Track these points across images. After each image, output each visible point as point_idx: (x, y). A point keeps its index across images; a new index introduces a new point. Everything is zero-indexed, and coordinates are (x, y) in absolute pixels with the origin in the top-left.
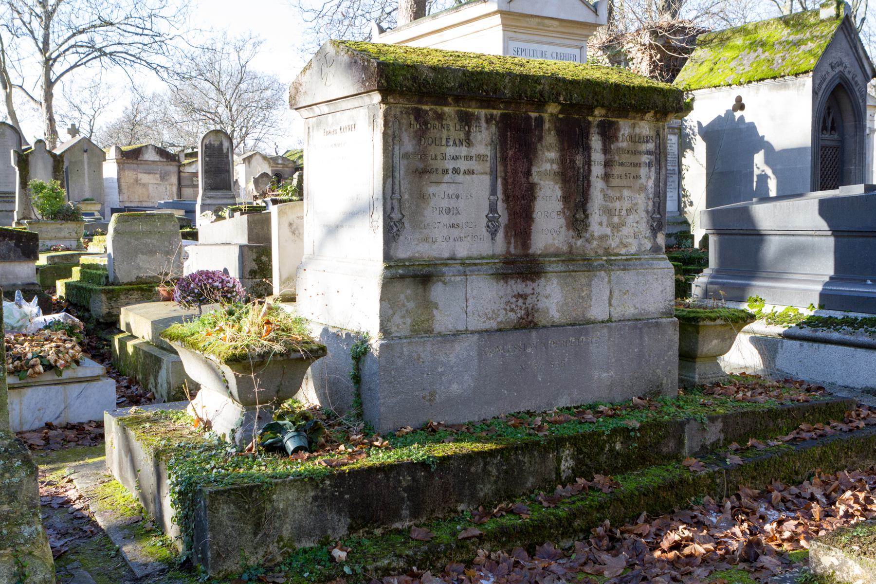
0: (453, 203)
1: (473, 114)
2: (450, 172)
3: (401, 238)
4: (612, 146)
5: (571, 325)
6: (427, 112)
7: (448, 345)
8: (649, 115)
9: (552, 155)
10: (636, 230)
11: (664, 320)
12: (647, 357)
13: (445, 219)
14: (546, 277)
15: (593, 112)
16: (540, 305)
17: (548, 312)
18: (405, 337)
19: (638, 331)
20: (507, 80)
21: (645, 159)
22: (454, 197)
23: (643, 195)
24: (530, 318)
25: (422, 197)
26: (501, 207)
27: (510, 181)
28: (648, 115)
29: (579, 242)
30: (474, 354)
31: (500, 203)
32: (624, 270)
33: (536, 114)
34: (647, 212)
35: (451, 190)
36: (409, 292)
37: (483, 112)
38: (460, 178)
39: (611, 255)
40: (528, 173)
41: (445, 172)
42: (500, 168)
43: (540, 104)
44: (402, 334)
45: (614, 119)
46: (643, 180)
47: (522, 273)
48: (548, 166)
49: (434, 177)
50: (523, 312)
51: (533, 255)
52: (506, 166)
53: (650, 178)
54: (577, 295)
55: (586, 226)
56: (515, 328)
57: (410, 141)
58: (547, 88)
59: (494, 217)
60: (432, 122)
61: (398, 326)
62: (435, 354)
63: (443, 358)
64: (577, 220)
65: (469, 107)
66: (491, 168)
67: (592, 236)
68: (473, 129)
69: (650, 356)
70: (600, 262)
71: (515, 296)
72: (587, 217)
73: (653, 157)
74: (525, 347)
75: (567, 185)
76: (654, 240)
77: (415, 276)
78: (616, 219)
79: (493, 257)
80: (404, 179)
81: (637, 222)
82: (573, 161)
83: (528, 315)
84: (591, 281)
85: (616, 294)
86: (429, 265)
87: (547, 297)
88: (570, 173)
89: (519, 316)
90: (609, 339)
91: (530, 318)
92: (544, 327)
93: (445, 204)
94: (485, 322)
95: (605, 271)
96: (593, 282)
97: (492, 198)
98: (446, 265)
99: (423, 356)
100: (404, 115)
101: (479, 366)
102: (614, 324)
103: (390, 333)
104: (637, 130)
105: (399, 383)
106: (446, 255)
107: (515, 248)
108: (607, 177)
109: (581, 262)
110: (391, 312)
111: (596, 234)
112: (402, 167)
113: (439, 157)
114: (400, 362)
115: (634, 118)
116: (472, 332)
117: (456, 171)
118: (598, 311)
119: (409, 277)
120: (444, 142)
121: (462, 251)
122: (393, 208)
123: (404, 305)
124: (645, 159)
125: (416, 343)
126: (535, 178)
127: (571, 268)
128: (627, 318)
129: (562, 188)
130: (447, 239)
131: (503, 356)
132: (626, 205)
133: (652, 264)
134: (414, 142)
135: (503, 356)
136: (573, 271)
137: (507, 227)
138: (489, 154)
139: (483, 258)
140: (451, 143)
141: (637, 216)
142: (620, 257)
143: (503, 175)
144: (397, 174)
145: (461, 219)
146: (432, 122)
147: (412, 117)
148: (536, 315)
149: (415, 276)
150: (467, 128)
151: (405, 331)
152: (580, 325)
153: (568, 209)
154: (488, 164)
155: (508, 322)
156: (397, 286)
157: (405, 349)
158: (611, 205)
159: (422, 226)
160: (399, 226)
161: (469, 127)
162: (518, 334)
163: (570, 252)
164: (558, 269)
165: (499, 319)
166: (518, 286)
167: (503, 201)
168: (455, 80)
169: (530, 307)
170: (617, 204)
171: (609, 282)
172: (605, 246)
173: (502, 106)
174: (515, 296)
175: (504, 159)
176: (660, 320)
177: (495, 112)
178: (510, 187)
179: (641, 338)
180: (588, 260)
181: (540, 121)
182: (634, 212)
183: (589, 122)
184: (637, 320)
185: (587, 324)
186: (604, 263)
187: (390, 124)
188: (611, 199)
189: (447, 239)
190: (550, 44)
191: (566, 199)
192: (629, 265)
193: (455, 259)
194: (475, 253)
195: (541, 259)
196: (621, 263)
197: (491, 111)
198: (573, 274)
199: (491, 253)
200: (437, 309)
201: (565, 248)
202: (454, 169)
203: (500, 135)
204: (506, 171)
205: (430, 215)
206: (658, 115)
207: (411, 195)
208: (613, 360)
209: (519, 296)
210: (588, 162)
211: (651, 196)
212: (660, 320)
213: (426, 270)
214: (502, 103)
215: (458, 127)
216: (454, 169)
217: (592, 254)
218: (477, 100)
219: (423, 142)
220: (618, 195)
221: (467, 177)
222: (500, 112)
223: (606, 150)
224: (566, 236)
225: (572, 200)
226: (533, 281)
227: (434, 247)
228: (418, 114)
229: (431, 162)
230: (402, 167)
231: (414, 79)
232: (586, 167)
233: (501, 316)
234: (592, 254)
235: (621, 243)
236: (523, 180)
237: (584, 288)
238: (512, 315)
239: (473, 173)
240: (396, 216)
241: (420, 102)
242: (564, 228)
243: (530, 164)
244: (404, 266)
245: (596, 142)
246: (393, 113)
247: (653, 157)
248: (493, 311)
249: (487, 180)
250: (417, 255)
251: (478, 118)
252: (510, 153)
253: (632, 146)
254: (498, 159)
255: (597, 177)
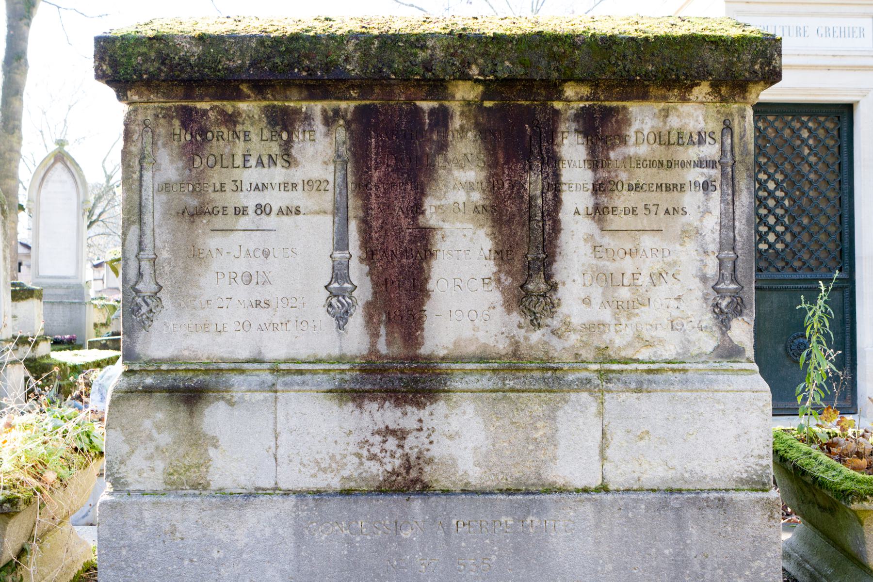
0: (256, 265)
1: (297, 111)
2: (251, 211)
3: (155, 323)
4: (612, 155)
5: (508, 492)
6: (205, 112)
7: (232, 514)
8: (702, 90)
9: (473, 174)
10: (676, 313)
11: (741, 496)
12: (697, 568)
13: (241, 292)
14: (448, 400)
15: (562, 92)
16: (435, 451)
17: (454, 464)
18: (154, 493)
19: (671, 514)
20: (350, 47)
21: (696, 175)
22: (259, 253)
23: (691, 246)
24: (413, 474)
25: (197, 255)
26: (358, 272)
27: (376, 224)
28: (696, 91)
29: (536, 336)
30: (286, 532)
31: (354, 264)
32: (638, 390)
33: (435, 104)
34: (704, 279)
35: (254, 241)
36: (160, 416)
37: (317, 107)
38: (271, 221)
39: (612, 361)
40: (417, 209)
41: (241, 211)
42: (354, 203)
43: (437, 87)
44: (148, 487)
45: (615, 104)
46: (692, 218)
47: (395, 391)
48: (460, 196)
49: (219, 221)
50: (397, 462)
51: (429, 358)
52: (366, 198)
53: (708, 211)
54: (521, 435)
55: (552, 307)
56: (380, 491)
57: (172, 162)
58: (439, 54)
59: (345, 290)
60: (215, 129)
61: (140, 473)
62: (206, 527)
63: (223, 535)
64: (528, 294)
65: (287, 99)
66: (335, 202)
67: (567, 324)
68: (298, 137)
69: (703, 566)
70: (584, 374)
71: (379, 432)
72: (554, 287)
73: (715, 173)
74: (397, 526)
75: (505, 229)
76: (724, 333)
77: (172, 390)
78: (624, 293)
79: (340, 359)
80: (160, 226)
81: (678, 298)
82: (517, 186)
83: (408, 468)
84: (554, 410)
85: (617, 437)
86: (207, 371)
87: (451, 437)
88: (511, 207)
89: (389, 468)
90: (597, 526)
91: (413, 474)
92: (446, 492)
93: (240, 266)
94: (314, 476)
95: (591, 392)
96: (560, 413)
97: (337, 255)
98: (242, 371)
99: (180, 527)
100: (162, 121)
101: (297, 556)
102: (610, 497)
103: (126, 484)
104: (674, 122)
105: (136, 571)
106: (244, 354)
107: (389, 344)
108: (599, 212)
109: (537, 374)
110: (126, 448)
111: (576, 321)
112: (158, 206)
113: (229, 187)
114: (137, 536)
115: (665, 98)
116: (287, 493)
117: (262, 210)
118: (573, 466)
119: (162, 390)
120: (239, 161)
121: (276, 348)
122: (140, 275)
123: (150, 438)
124: (696, 175)
125: (167, 505)
126: (431, 216)
127: (510, 384)
128: (647, 486)
129: (493, 236)
130: (245, 326)
131: (350, 541)
132: (649, 265)
133: (711, 382)
134: (181, 164)
135: (350, 541)
136: (512, 390)
137: (371, 309)
138: (331, 179)
139: (320, 361)
140: (253, 162)
141: (677, 286)
142: (633, 366)
143: (361, 213)
144: (147, 218)
145: (271, 293)
146: (215, 129)
147: (177, 123)
148: (427, 469)
149: (172, 390)
150: (285, 136)
151: (154, 480)
152: (528, 493)
153: (508, 273)
154: (329, 197)
155: (364, 480)
156: (138, 406)
157: (146, 514)
158: (610, 266)
159: (197, 303)
160: (152, 305)
161: (290, 134)
162: (382, 501)
163: (515, 354)
164: (479, 386)
165: (346, 473)
166: (389, 415)
167: (361, 260)
168: (243, 54)
169: (413, 455)
170: (628, 265)
171: (601, 414)
172: (597, 342)
173: (353, 94)
174: (379, 432)
175: (363, 186)
176: (727, 496)
177: (343, 105)
178: (375, 236)
179: (680, 527)
180: (555, 370)
181: (442, 117)
182: (669, 278)
183: (557, 112)
184: (671, 491)
185: (548, 491)
186: (594, 376)
187: (135, 137)
188: (611, 254)
189: (245, 326)
190: (813, 14)
191: (502, 255)
192: (650, 382)
193: (261, 362)
194: (303, 353)
195: (443, 365)
196: (634, 376)
197: (335, 103)
198: (513, 395)
199: (335, 352)
200: (216, 447)
201: (502, 346)
202: (259, 206)
203: (353, 145)
204: (366, 208)
205: (210, 283)
206: (724, 90)
207: (173, 252)
208: (609, 567)
209: (388, 432)
210: (555, 187)
211: (713, 247)
212: (727, 496)
213: (196, 380)
214: (353, 87)
215: (266, 134)
216: (259, 206)
217: (567, 357)
218: (300, 86)
219: (197, 163)
220: (628, 246)
221: (285, 218)
222: (353, 104)
223: (595, 162)
224: (505, 325)
225: (518, 257)
226: (420, 405)
227: (220, 339)
228: (188, 117)
229: (213, 195)
230: (158, 206)
231: (163, 59)
232: (550, 195)
233: (349, 467)
234: (567, 357)
235: (639, 337)
236: (404, 222)
237: (540, 424)
238: (374, 468)
239: (298, 212)
240: (146, 287)
241: (188, 97)
242: (500, 309)
243: (421, 192)
244: (159, 371)
245: (572, 149)
246: (140, 118)
247: (715, 173)
248: (332, 458)
249: (326, 225)
250: (186, 353)
251: (308, 118)
252: (376, 175)
253: (660, 153)
254: (351, 186)
255: (577, 212)
